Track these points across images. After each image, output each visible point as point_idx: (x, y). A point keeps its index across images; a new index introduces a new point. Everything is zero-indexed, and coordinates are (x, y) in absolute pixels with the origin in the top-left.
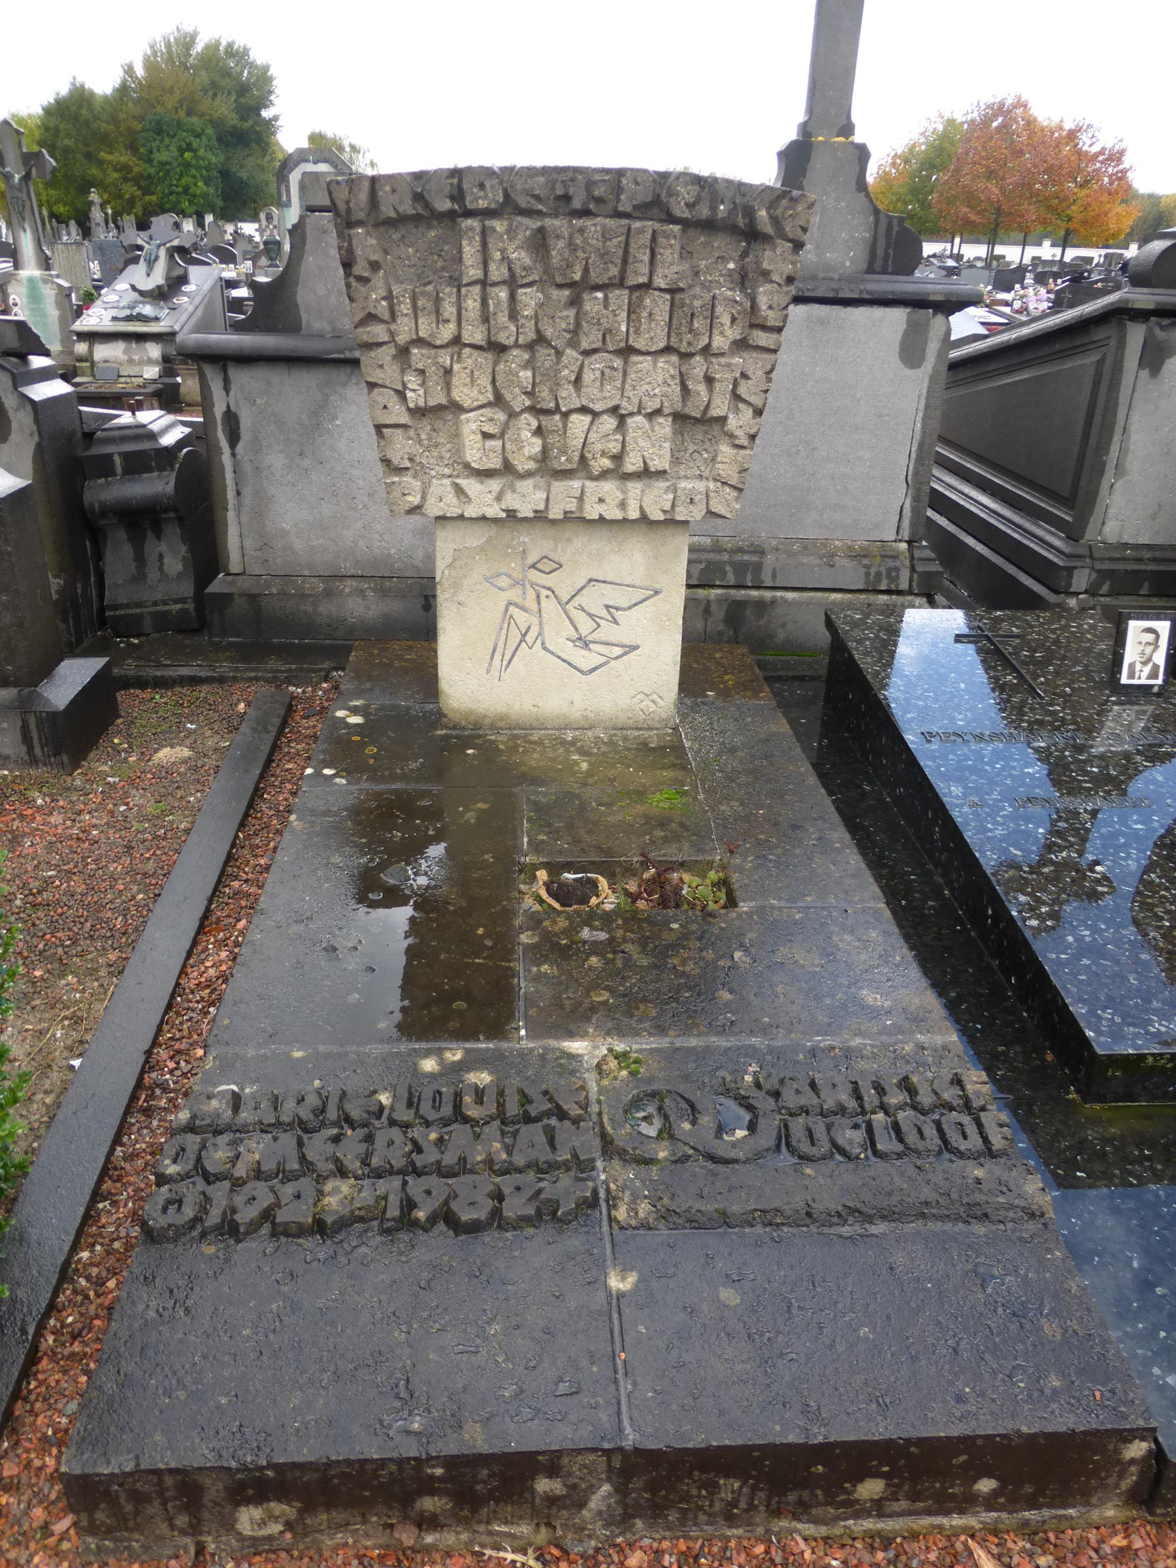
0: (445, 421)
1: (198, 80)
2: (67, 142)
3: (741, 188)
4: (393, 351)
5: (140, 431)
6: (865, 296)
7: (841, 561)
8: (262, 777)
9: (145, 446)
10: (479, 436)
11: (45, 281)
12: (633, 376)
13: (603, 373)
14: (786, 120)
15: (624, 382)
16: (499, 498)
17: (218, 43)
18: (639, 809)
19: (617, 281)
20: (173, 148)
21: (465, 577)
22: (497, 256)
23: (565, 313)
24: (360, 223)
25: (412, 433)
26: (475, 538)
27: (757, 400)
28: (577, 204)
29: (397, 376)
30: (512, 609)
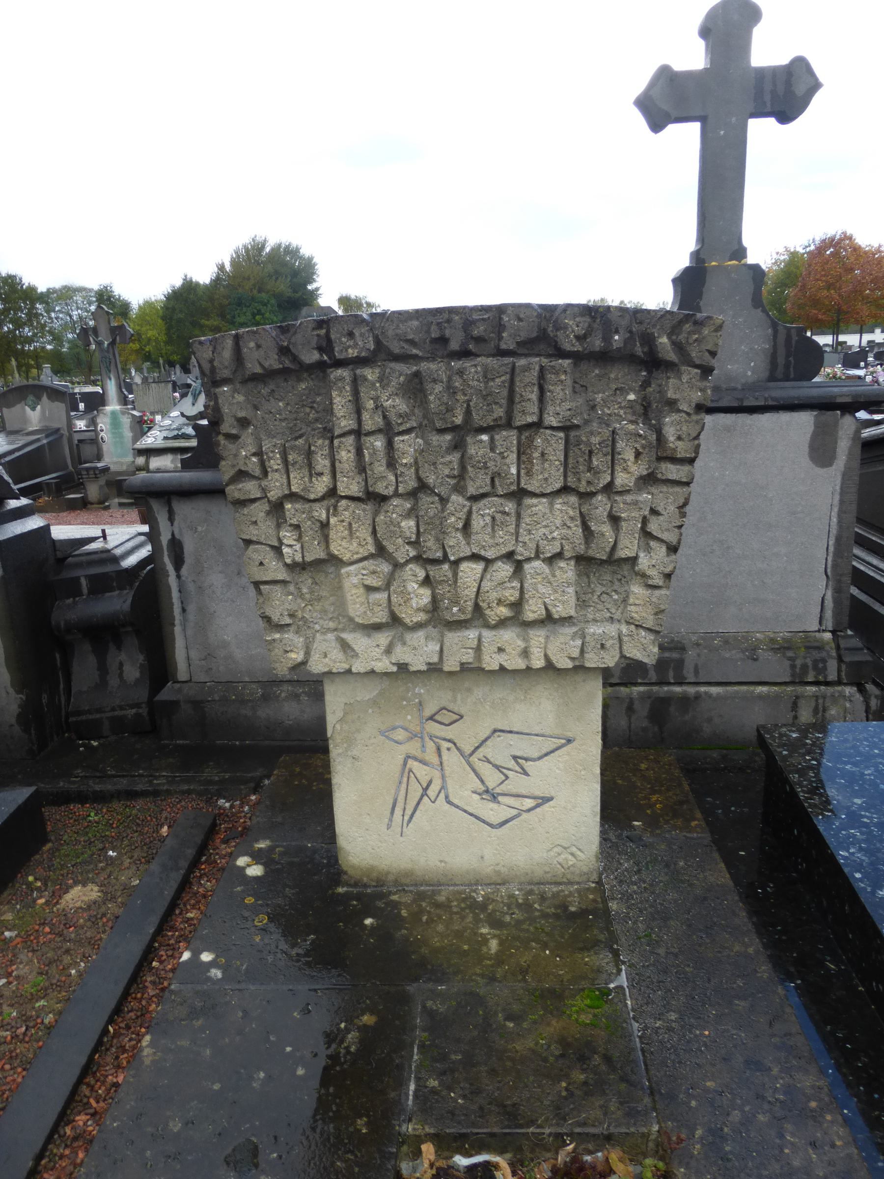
0: (327, 574)
1: (266, 270)
2: (181, 316)
3: (638, 314)
4: (266, 507)
5: (104, 555)
6: (771, 403)
7: (764, 654)
8: (159, 930)
9: (109, 568)
10: (362, 590)
11: (123, 413)
12: (528, 520)
13: (493, 518)
14: (679, 247)
15: (518, 526)
16: (388, 651)
17: (280, 245)
18: (556, 1025)
19: (503, 421)
20: (249, 314)
21: (358, 731)
22: (370, 404)
23: (448, 458)
24: (225, 381)
25: (292, 588)
26: (366, 693)
27: (671, 537)
28: (454, 346)
29: (272, 531)
30: (411, 763)
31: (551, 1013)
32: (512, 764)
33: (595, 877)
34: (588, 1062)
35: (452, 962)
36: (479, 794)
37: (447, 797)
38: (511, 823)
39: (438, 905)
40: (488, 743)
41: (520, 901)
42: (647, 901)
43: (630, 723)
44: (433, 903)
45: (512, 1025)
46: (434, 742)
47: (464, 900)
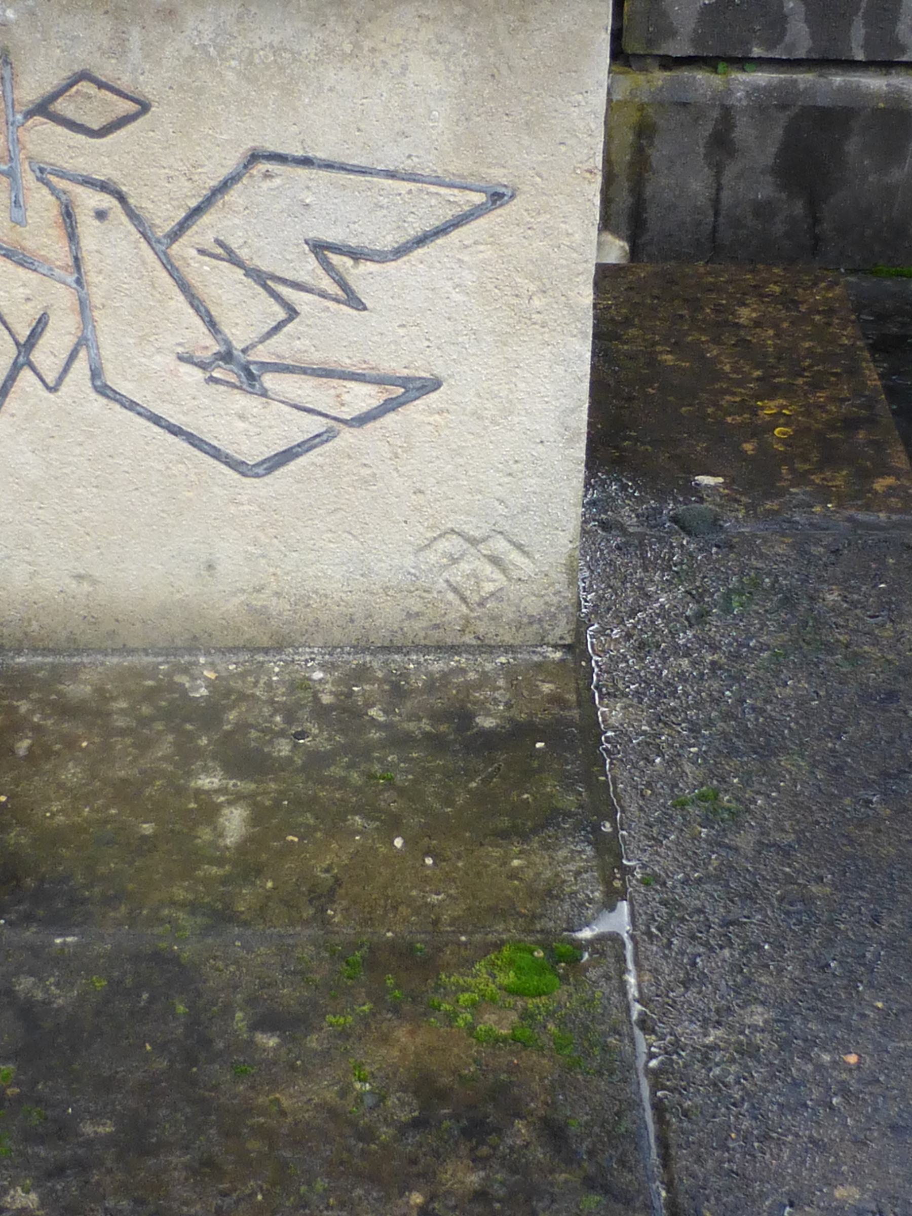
18: (405, 1041)
31: (396, 1009)
32: (308, 269)
33: (562, 630)
34: (493, 1138)
35: (102, 869)
36: (202, 366)
37: (96, 373)
38: (302, 461)
39: (67, 710)
40: (233, 196)
41: (326, 699)
42: (716, 701)
43: (719, 188)
44: (53, 704)
45: (272, 1042)
46: (53, 190)
47: (150, 695)
